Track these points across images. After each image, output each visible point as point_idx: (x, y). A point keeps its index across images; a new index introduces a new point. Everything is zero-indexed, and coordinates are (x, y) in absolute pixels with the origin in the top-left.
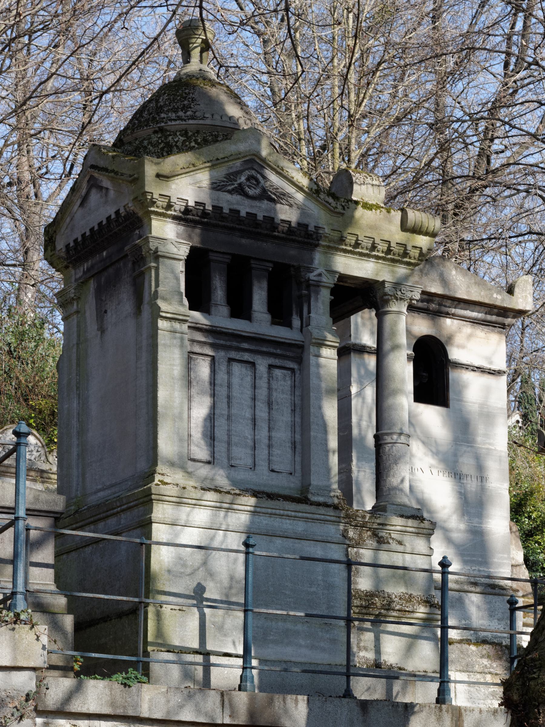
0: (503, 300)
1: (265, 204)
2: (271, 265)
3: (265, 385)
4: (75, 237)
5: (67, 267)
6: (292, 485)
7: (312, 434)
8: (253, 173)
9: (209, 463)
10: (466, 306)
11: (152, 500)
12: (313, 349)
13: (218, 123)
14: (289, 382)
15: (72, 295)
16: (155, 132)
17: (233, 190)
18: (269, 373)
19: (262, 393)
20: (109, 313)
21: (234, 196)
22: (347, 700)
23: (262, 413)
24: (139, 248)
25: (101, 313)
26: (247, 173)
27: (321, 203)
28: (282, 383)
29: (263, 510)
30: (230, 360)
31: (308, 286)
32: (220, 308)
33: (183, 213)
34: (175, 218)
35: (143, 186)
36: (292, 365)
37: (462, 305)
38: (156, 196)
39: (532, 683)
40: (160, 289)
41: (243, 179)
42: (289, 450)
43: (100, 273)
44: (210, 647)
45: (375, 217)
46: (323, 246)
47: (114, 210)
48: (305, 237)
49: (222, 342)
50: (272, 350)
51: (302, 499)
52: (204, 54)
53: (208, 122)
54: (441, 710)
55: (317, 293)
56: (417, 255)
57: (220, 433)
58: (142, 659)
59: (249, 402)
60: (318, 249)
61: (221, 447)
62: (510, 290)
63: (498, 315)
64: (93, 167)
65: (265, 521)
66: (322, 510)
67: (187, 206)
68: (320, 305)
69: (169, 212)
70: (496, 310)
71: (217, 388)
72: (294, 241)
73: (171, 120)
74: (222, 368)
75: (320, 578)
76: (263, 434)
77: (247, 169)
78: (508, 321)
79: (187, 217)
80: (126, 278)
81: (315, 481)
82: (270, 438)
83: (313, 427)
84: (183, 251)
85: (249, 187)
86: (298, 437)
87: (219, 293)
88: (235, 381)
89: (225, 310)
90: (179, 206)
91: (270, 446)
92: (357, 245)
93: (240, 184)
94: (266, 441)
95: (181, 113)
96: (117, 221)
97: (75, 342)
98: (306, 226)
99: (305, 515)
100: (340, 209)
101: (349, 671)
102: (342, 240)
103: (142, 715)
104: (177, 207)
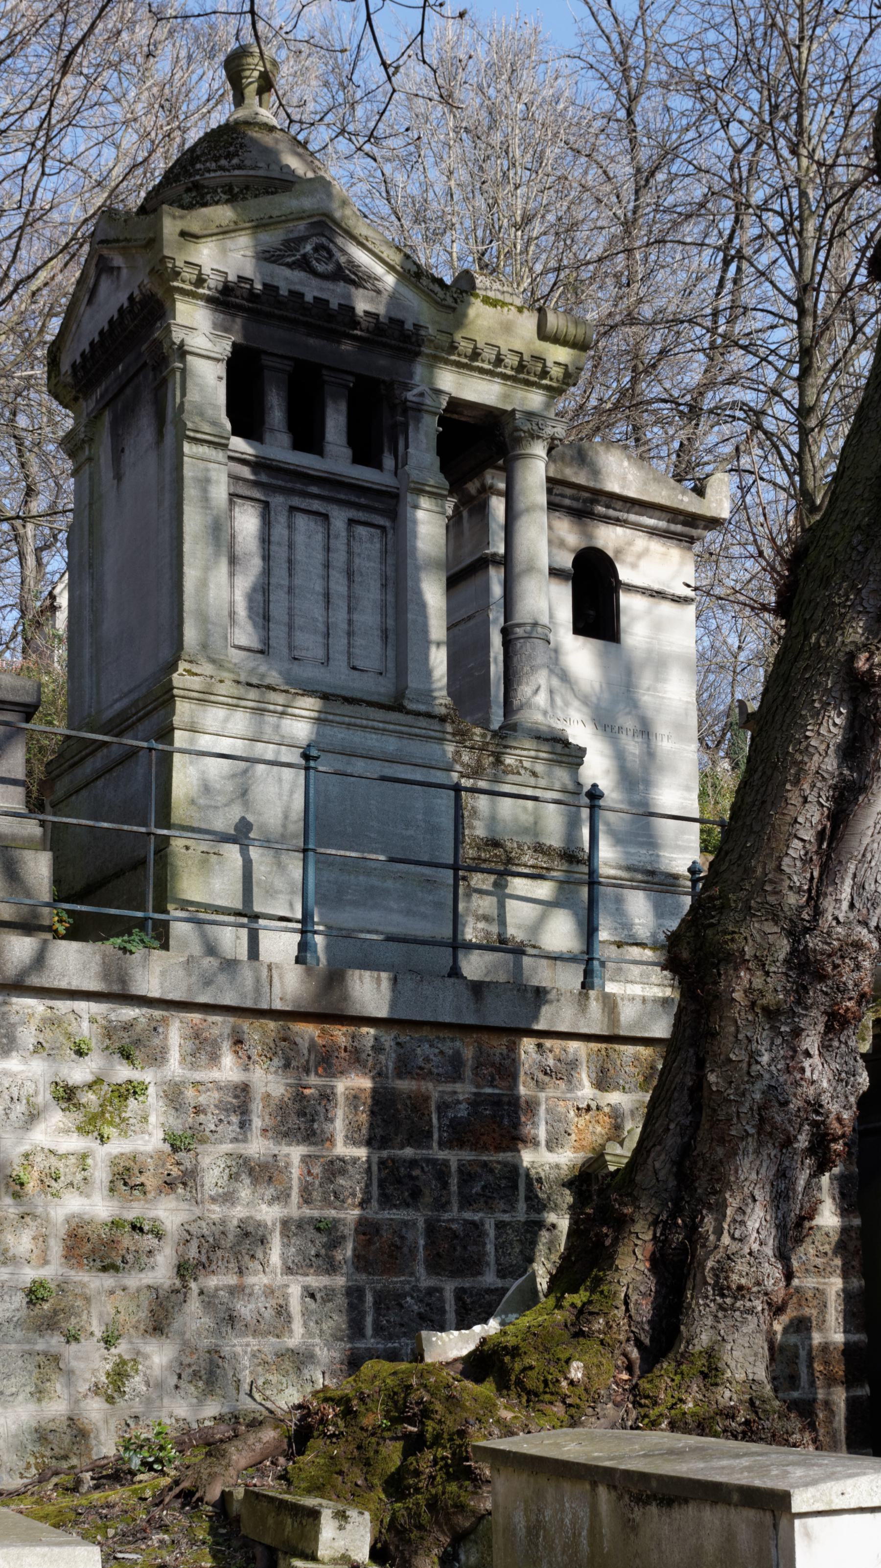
0: (690, 502)
4: (81, 350)
5: (76, 399)
6: (382, 690)
7: (410, 616)
8: (324, 240)
9: (262, 652)
10: (642, 510)
11: (174, 696)
12: (410, 497)
13: (276, 175)
14: (378, 546)
15: (82, 436)
16: (188, 190)
17: (294, 263)
19: (339, 558)
20: (127, 452)
22: (452, 980)
23: (339, 585)
24: (158, 344)
25: (118, 452)
26: (315, 240)
27: (423, 291)
28: (368, 545)
29: (338, 719)
30: (293, 509)
31: (405, 411)
32: (278, 435)
34: (209, 300)
35: (161, 250)
37: (637, 508)
38: (179, 263)
39: (709, 932)
41: (308, 248)
42: (378, 640)
44: (257, 908)
46: (428, 355)
47: (127, 296)
48: (399, 340)
49: (280, 483)
50: (353, 498)
51: (396, 705)
53: (261, 173)
54: (587, 997)
55: (418, 420)
56: (561, 375)
57: (278, 611)
58: (152, 915)
59: (320, 570)
61: (278, 633)
62: (700, 491)
63: (684, 524)
64: (102, 242)
65: (339, 735)
66: (423, 722)
68: (422, 437)
70: (681, 518)
71: (273, 548)
73: (209, 171)
76: (340, 616)
77: (316, 235)
78: (695, 532)
79: (228, 299)
80: (147, 396)
81: (413, 682)
82: (350, 622)
83: (410, 607)
84: (224, 347)
85: (317, 260)
86: (391, 622)
87: (276, 412)
88: (300, 539)
89: (285, 439)
90: (214, 282)
91: (350, 634)
92: (476, 355)
93: (304, 256)
94: (345, 626)
95: (223, 162)
97: (87, 502)
98: (401, 323)
99: (398, 728)
100: (450, 301)
102: (453, 348)
103: (150, 995)
104: (212, 283)
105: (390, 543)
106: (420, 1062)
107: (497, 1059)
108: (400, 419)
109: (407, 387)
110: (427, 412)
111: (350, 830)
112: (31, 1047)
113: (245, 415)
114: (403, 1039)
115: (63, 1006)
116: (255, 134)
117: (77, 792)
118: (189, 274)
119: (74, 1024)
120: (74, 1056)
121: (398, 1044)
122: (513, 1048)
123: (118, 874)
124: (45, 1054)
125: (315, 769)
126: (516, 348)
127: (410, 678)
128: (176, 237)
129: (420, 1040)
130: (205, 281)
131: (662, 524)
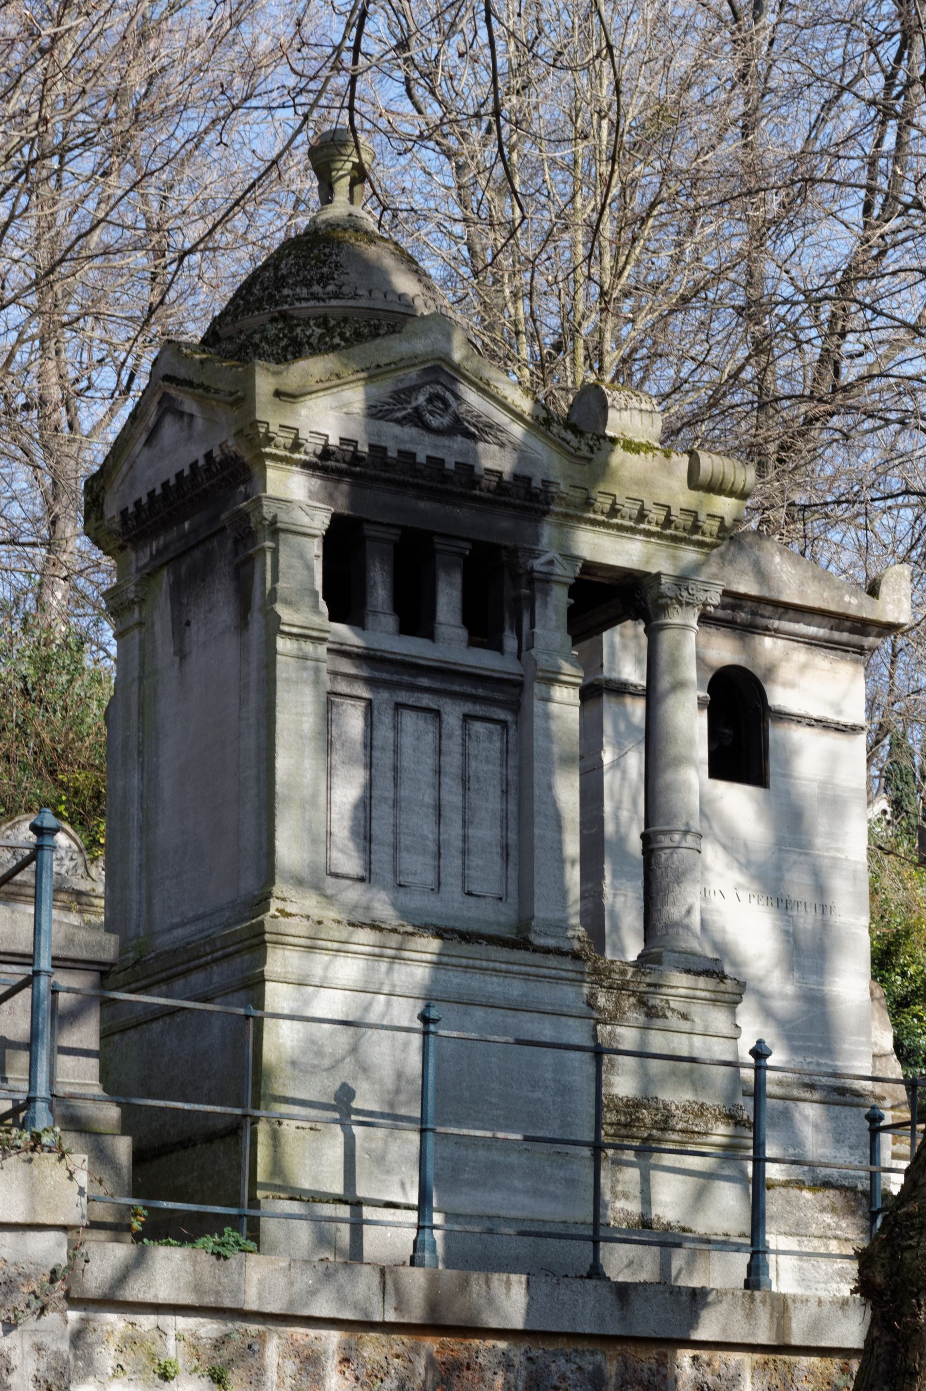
0: (860, 606)
1: (459, 442)
2: (468, 545)
3: (458, 749)
5: (122, 548)
6: (502, 919)
7: (536, 831)
8: (439, 389)
9: (361, 880)
10: (798, 616)
12: (538, 688)
13: (380, 305)
14: (498, 744)
16: (273, 320)
17: (404, 418)
18: (464, 728)
19: (452, 762)
22: (594, 1282)
23: (452, 796)
24: (243, 517)
25: (180, 626)
26: (429, 389)
27: (554, 442)
28: (487, 745)
29: (454, 961)
30: (399, 707)
31: (531, 582)
32: (382, 618)
34: (305, 465)
35: (252, 411)
37: (791, 614)
38: (273, 428)
39: (908, 1255)
41: (421, 399)
42: (497, 859)
46: (557, 514)
47: (203, 452)
48: (526, 498)
49: (385, 676)
50: (469, 690)
51: (519, 940)
52: (357, 189)
53: (362, 303)
54: (752, 1299)
55: (546, 593)
56: (715, 529)
57: (382, 829)
58: (247, 1211)
59: (430, 778)
60: (548, 518)
61: (382, 854)
62: (873, 590)
63: (852, 631)
64: (167, 378)
65: (456, 979)
66: (553, 961)
68: (551, 613)
69: (297, 456)
71: (376, 754)
72: (506, 505)
73: (300, 300)
74: (385, 719)
76: (453, 831)
79: (327, 464)
80: (224, 567)
81: (542, 911)
82: (465, 838)
83: (537, 819)
84: (320, 521)
85: (432, 413)
86: (513, 837)
87: (380, 593)
88: (407, 741)
89: (389, 622)
90: (313, 445)
91: (465, 852)
92: (614, 511)
93: (416, 409)
94: (459, 844)
95: (316, 289)
98: (528, 480)
100: (585, 451)
101: (598, 1233)
102: (588, 504)
104: (310, 448)
105: (512, 740)
106: (555, 1381)
107: (645, 1376)
108: (525, 591)
109: (534, 554)
110: (557, 582)
111: (467, 1094)
112: (110, 1371)
113: (344, 599)
114: (535, 1353)
115: (147, 1321)
116: (349, 237)
117: (123, 1031)
118: (283, 439)
119: (159, 1342)
120: (158, 1381)
121: (530, 1359)
122: (664, 1365)
123: (186, 1143)
124: (125, 1379)
125: (435, 1033)
126: (662, 502)
127: (536, 906)
128: (271, 397)
129: (555, 1354)
130: (302, 445)
131: (821, 632)
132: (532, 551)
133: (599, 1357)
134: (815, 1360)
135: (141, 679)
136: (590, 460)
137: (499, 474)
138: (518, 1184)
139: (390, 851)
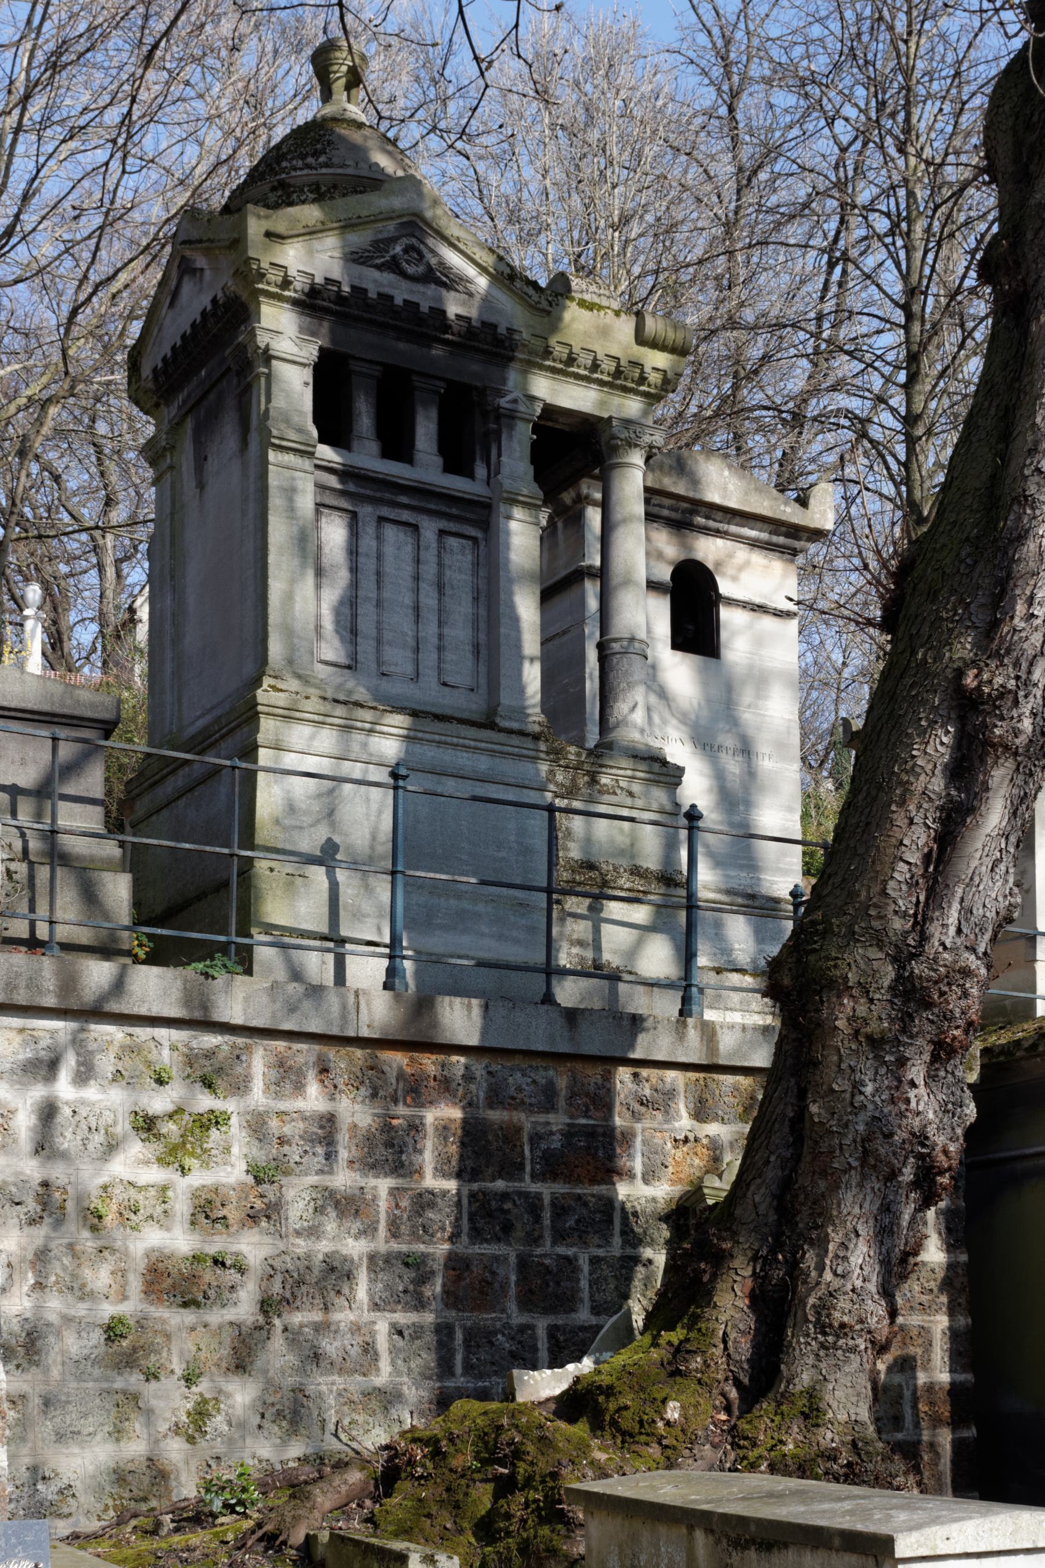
0: (793, 513)
1: (431, 289)
2: (443, 384)
3: (433, 560)
5: (157, 405)
6: (474, 707)
7: (502, 630)
9: (349, 667)
13: (365, 173)
16: (274, 189)
18: (440, 541)
19: (429, 570)
21: (385, 275)
22: (545, 1007)
23: (429, 599)
24: (243, 348)
25: (200, 460)
26: (405, 241)
29: (428, 736)
30: (381, 520)
33: (307, 295)
35: (245, 250)
36: (473, 532)
37: (738, 519)
38: (264, 265)
39: (812, 958)
40: (274, 404)
41: (398, 249)
42: (469, 656)
43: (199, 402)
44: (344, 932)
45: (595, 326)
46: (521, 360)
48: (492, 346)
50: (444, 509)
51: (488, 722)
52: (354, 91)
53: (350, 171)
54: (685, 1025)
55: (511, 428)
56: (659, 382)
57: (366, 624)
59: (409, 583)
60: (513, 365)
61: (366, 647)
62: (803, 502)
63: (787, 535)
65: (430, 754)
66: (515, 740)
67: (313, 285)
69: (287, 293)
71: (361, 559)
72: (477, 350)
73: (295, 169)
74: (369, 530)
75: (512, 838)
76: (430, 630)
78: (798, 544)
79: (315, 302)
80: (231, 402)
81: (506, 699)
82: (440, 637)
83: (503, 621)
84: (310, 352)
85: (408, 262)
86: (482, 637)
87: (365, 420)
88: (389, 550)
90: (300, 284)
91: (440, 649)
92: (571, 360)
93: (394, 257)
94: (435, 641)
95: (310, 160)
96: (214, 314)
98: (494, 327)
100: (544, 304)
101: (551, 971)
102: (547, 353)
103: (233, 1022)
104: (298, 286)
106: (512, 1091)
107: (592, 1088)
108: (493, 426)
109: (501, 394)
114: (494, 1067)
115: (143, 1033)
117: (158, 811)
118: (275, 276)
119: (155, 1051)
122: (608, 1078)
131: (764, 536)
132: (499, 391)
133: (551, 1073)
134: (740, 1078)
135: (172, 514)
136: (549, 313)
137: (468, 320)
138: (485, 929)
139: (374, 643)
